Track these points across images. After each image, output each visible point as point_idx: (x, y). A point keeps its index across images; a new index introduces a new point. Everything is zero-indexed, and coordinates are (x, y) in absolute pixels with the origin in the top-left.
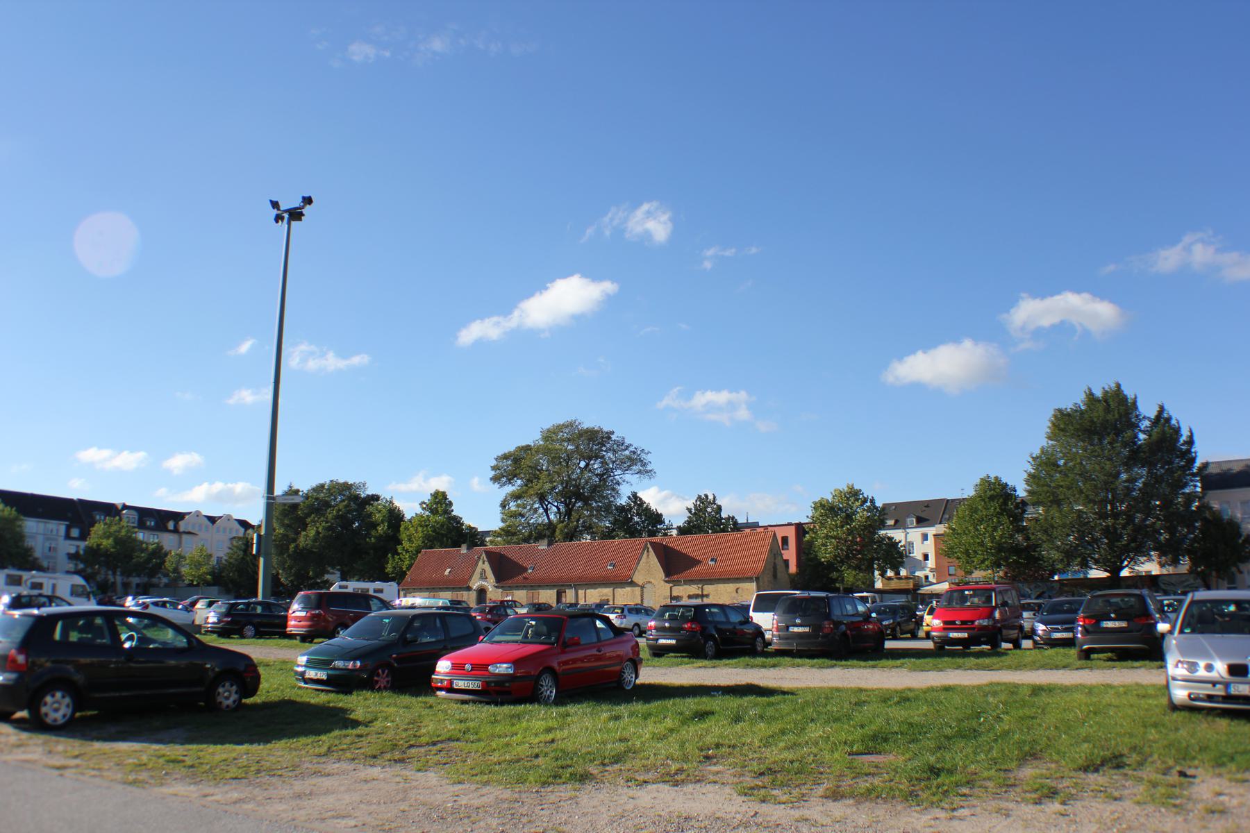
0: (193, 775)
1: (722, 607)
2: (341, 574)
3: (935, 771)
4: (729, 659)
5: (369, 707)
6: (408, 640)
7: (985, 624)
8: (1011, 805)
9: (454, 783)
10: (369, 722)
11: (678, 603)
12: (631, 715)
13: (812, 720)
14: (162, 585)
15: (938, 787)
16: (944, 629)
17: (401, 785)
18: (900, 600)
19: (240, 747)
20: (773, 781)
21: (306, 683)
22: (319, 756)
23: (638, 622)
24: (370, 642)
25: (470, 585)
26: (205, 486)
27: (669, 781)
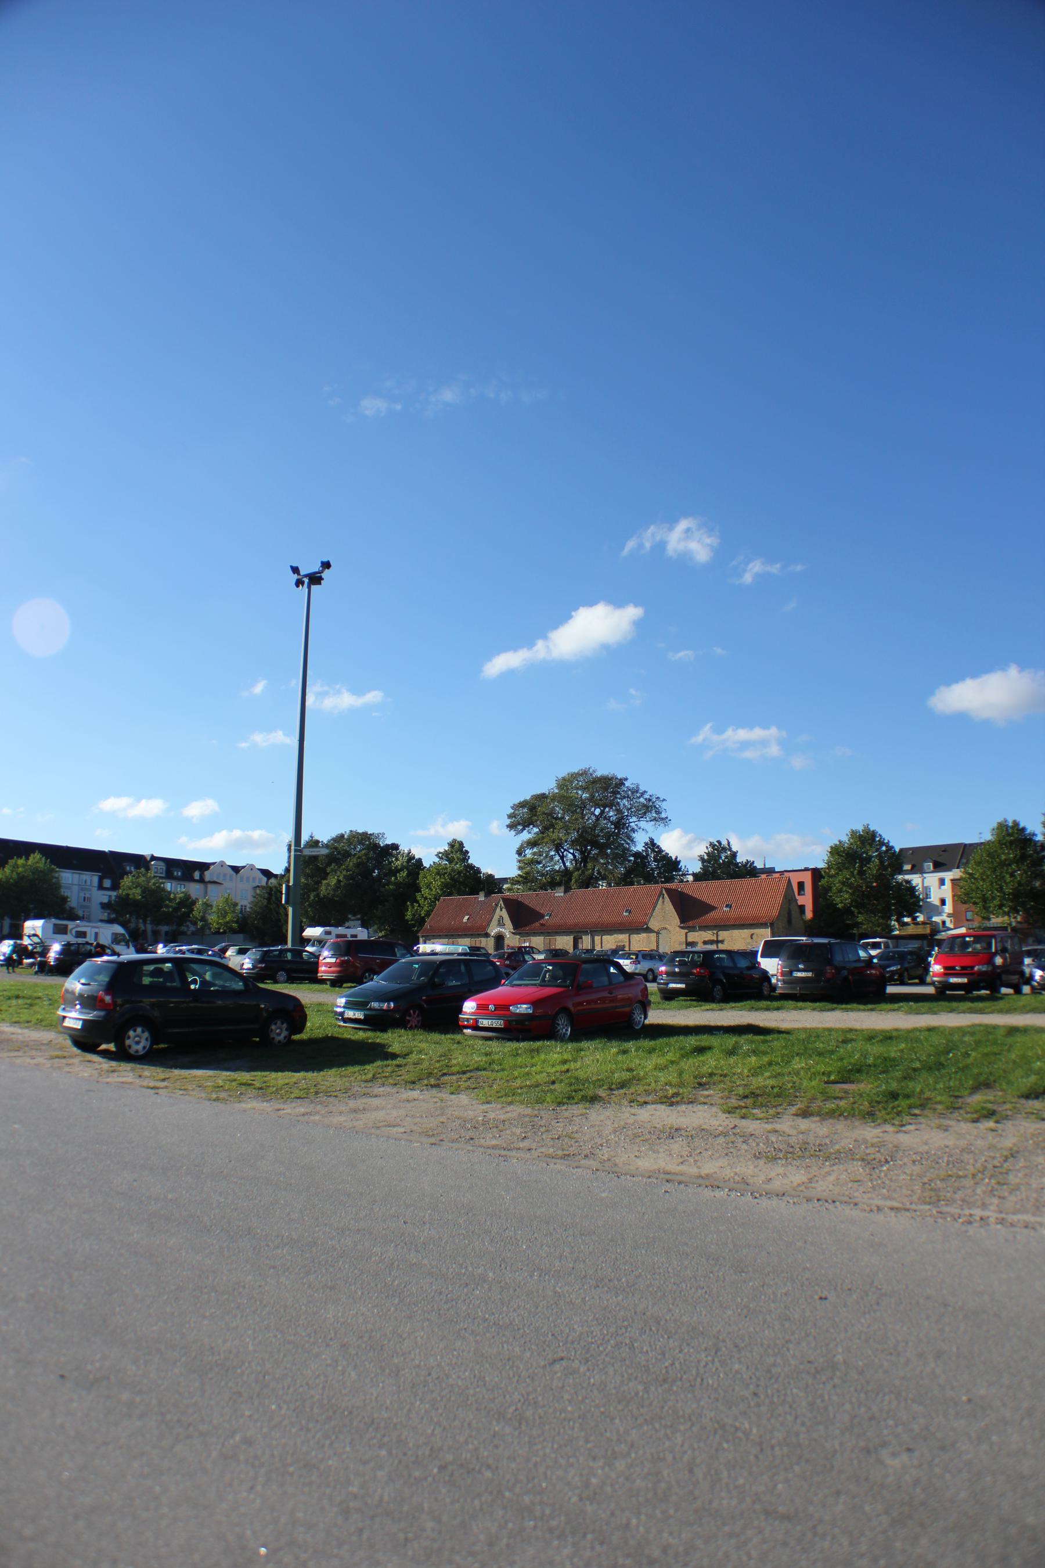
1: (729, 953)
3: (894, 1096)
7: (984, 969)
8: (951, 1123)
10: (406, 1055)
11: (694, 949)
13: (798, 1054)
14: (189, 933)
15: (893, 1108)
16: (945, 974)
17: (439, 1104)
18: (913, 945)
21: (345, 1022)
22: (366, 1081)
24: (402, 985)
26: (224, 833)
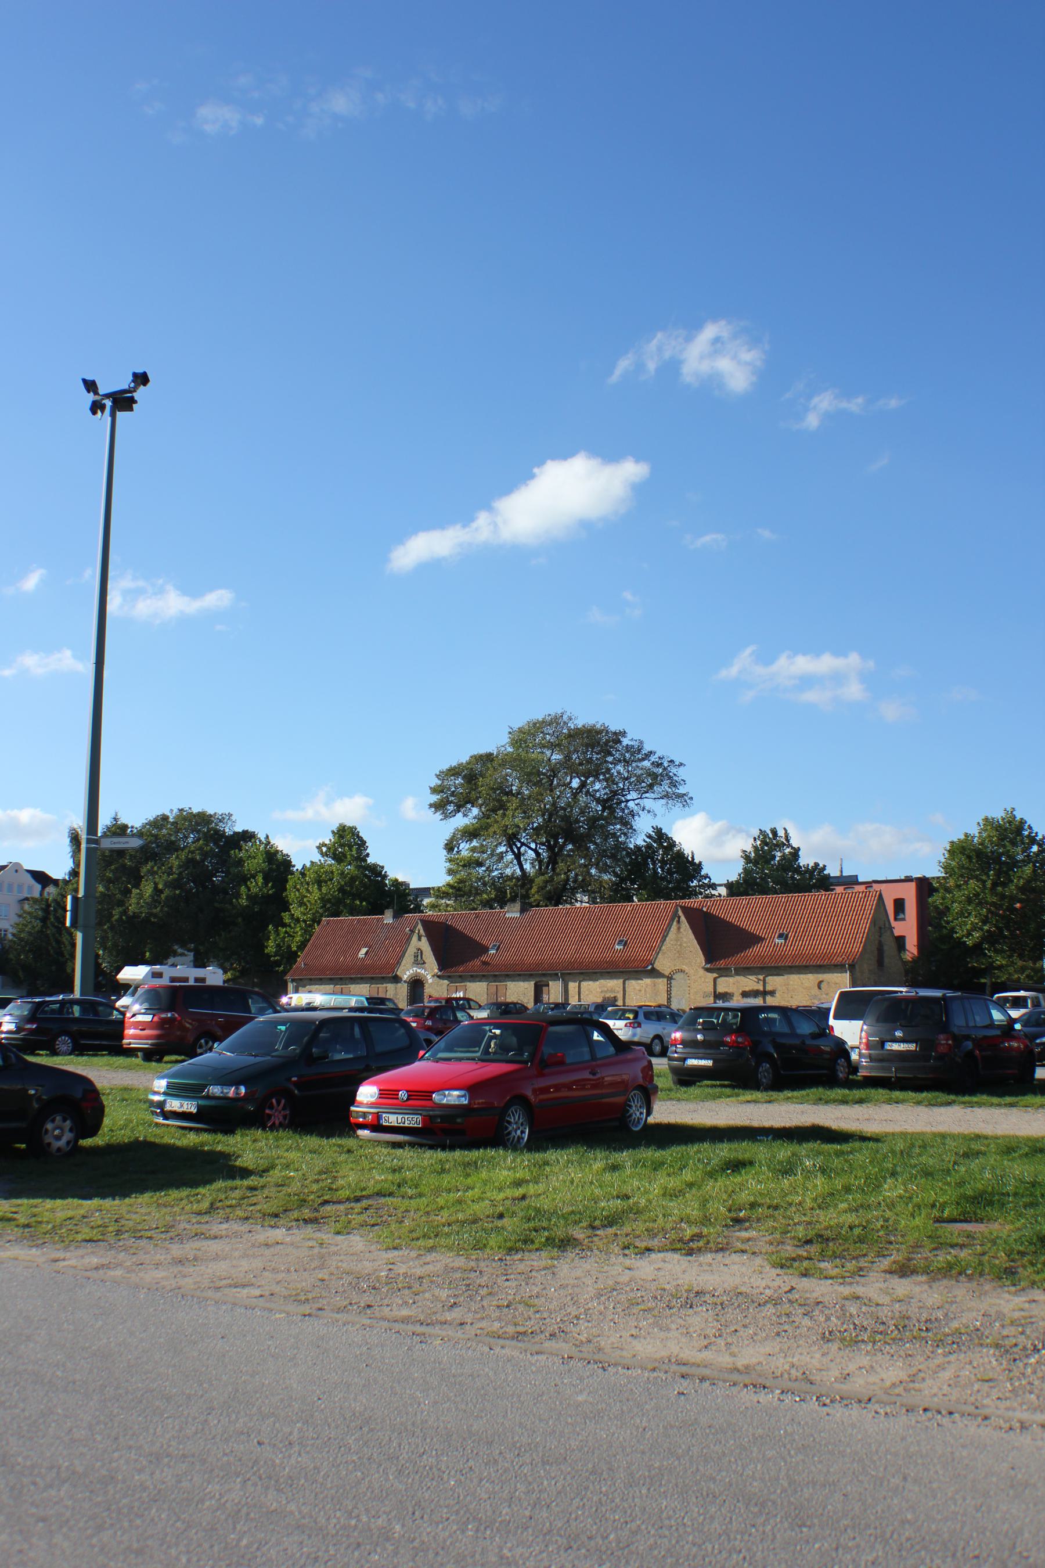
0: (31, 1236)
1: (783, 1011)
2: (195, 956)
4: (793, 1090)
5: (261, 1151)
6: (315, 1056)
9: (388, 1249)
10: (264, 1171)
11: (727, 1005)
12: (635, 1165)
17: (316, 1250)
19: (89, 1202)
20: (823, 1251)
22: (199, 1213)
23: (660, 1033)
24: (258, 1059)
25: (398, 973)
27: (680, 1249)
